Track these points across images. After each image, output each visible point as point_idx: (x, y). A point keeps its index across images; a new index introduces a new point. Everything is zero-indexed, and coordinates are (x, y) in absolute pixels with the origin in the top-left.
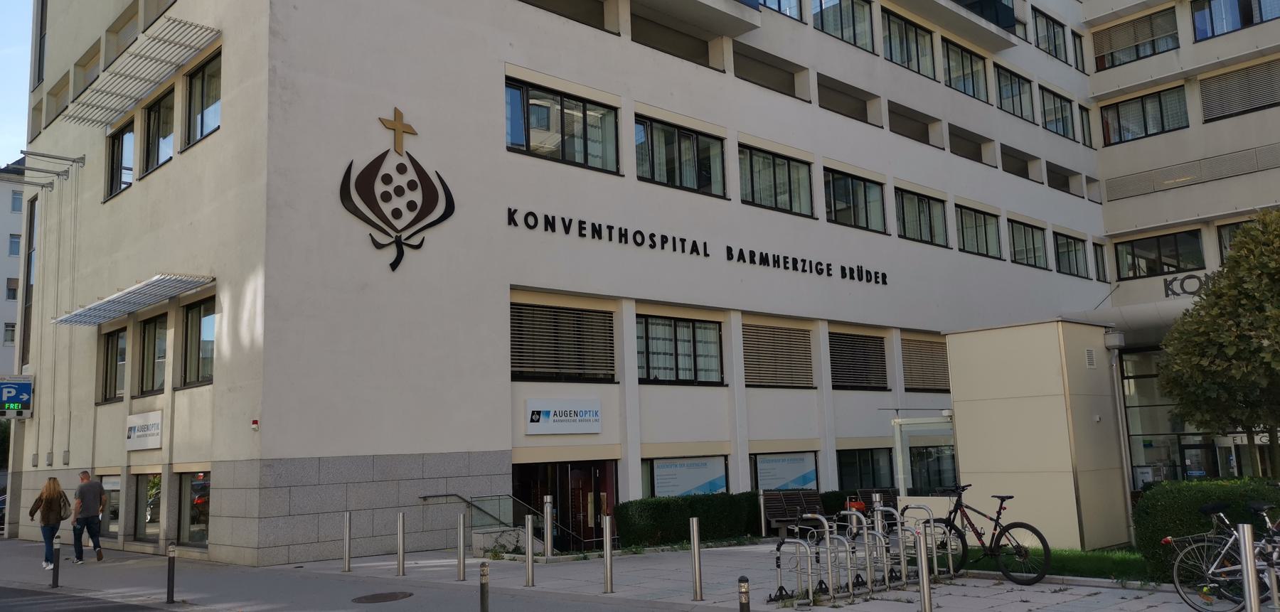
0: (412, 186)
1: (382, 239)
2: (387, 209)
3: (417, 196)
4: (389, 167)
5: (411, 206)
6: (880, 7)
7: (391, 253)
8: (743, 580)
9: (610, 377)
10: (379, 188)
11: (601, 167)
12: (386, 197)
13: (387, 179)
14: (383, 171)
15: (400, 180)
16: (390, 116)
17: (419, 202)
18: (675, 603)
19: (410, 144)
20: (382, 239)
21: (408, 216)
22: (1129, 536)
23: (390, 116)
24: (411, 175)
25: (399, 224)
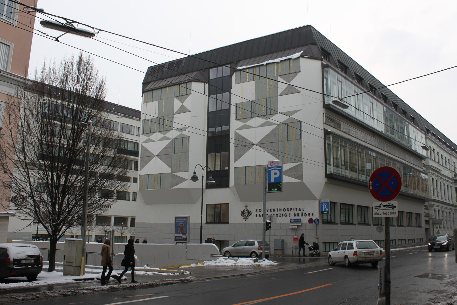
2: (245, 215)
4: (245, 211)
7: (245, 219)
10: (244, 213)
19: (247, 208)
21: (247, 215)
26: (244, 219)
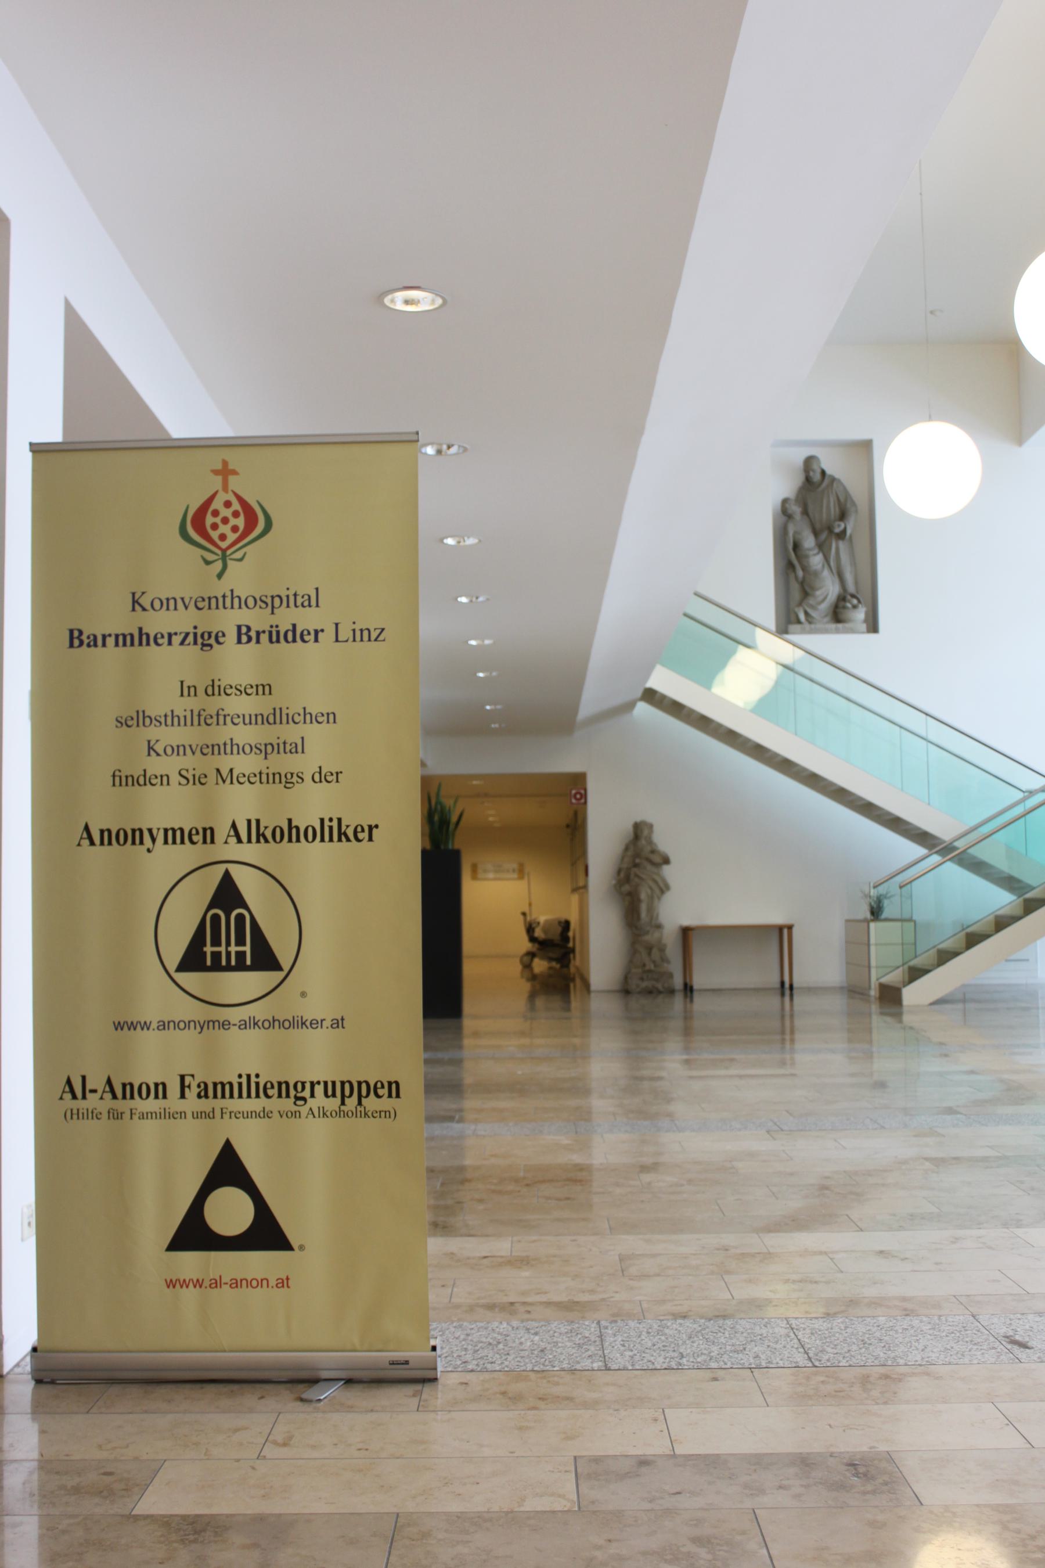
0: (236, 514)
1: (210, 557)
2: (215, 535)
3: (240, 522)
4: (217, 504)
5: (235, 529)
6: (294, 1241)
7: (218, 566)
8: (354, 623)
9: (581, 883)
10: (209, 520)
11: (765, 1548)
12: (215, 527)
13: (216, 513)
14: (213, 507)
15: (226, 513)
16: (219, 467)
17: (242, 526)
18: (555, 1511)
19: (233, 482)
20: (210, 557)
21: (232, 537)
22: (962, 847)
23: (219, 467)
24: (236, 506)
25: (224, 545)
26: (208, 563)
